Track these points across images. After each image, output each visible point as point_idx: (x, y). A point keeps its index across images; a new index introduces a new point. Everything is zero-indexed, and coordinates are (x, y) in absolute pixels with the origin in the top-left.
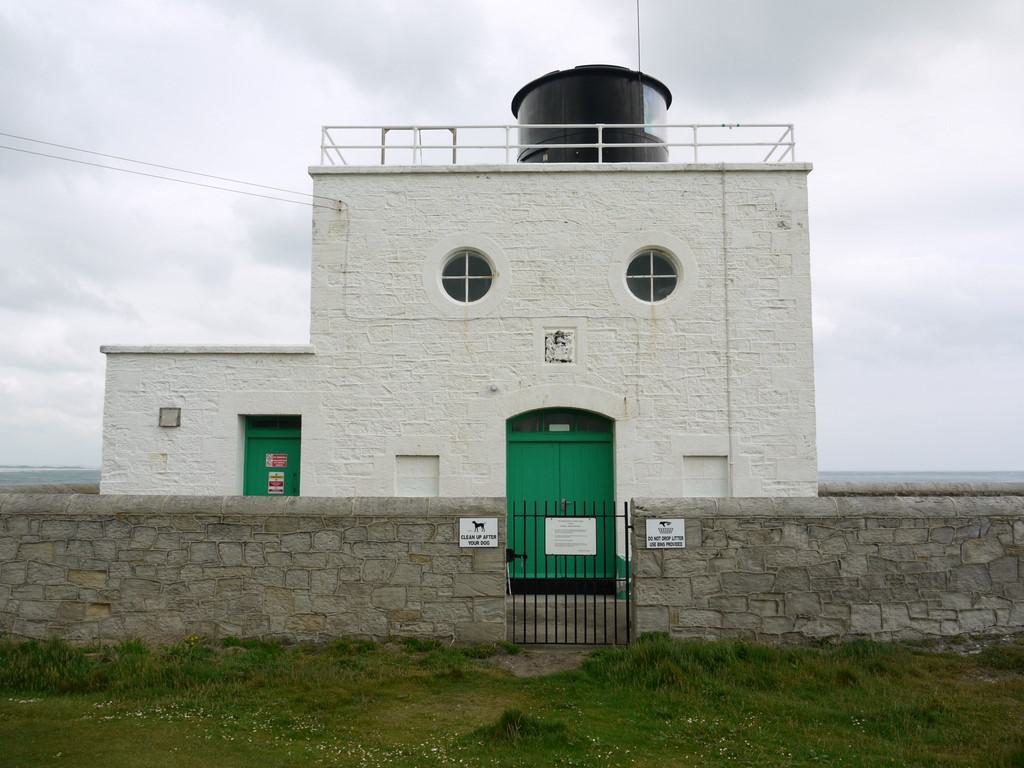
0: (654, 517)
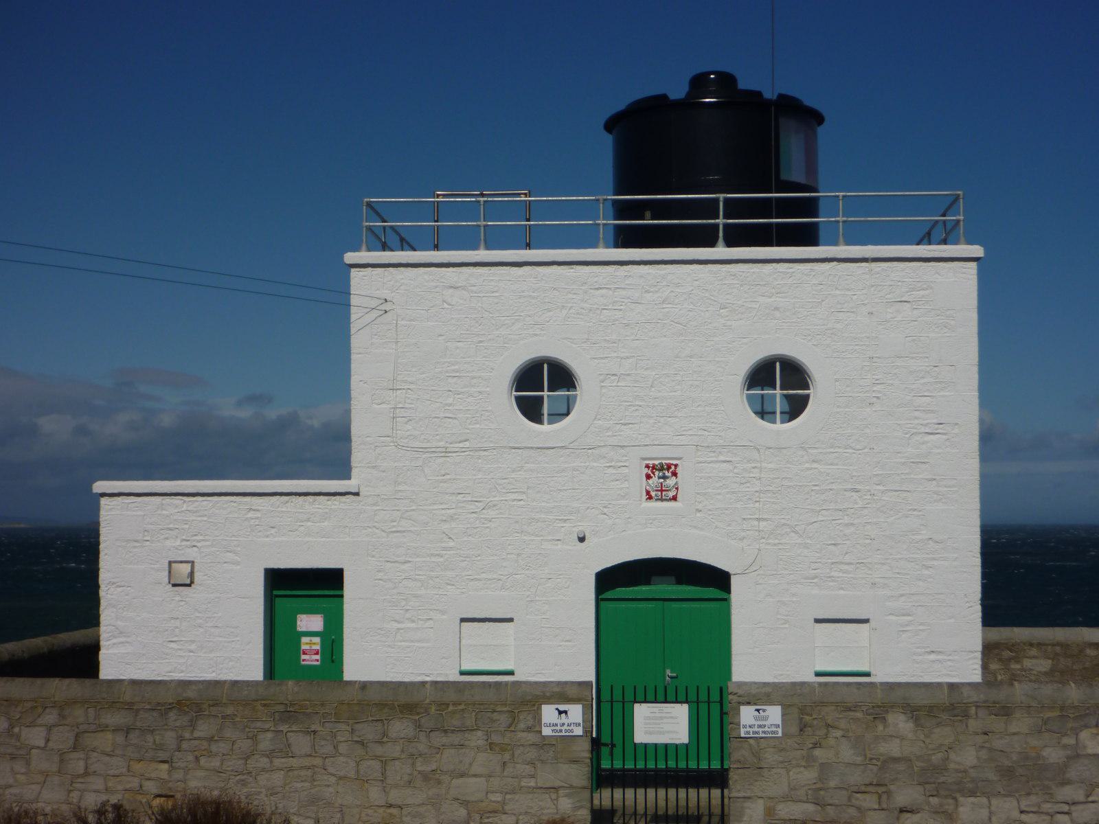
0: (749, 703)
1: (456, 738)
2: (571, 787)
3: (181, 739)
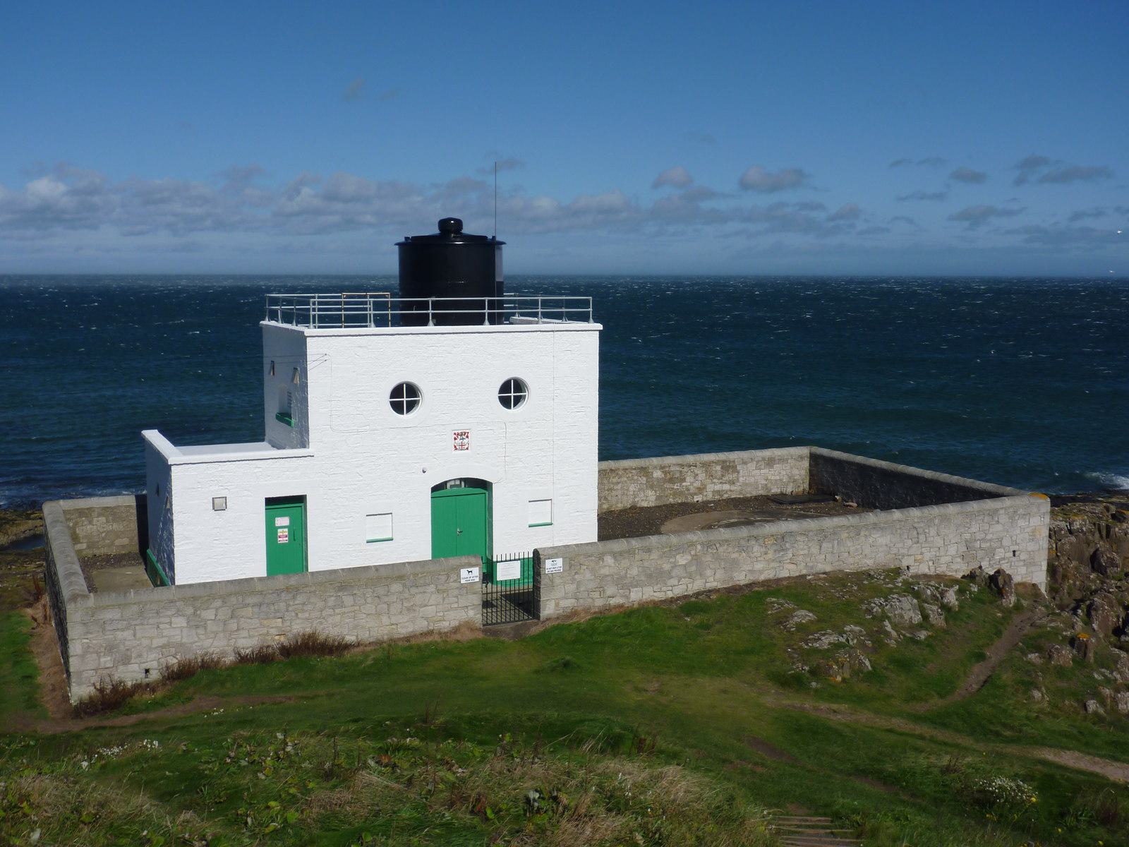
0: (549, 558)
1: (421, 589)
2: (474, 605)
3: (288, 606)
